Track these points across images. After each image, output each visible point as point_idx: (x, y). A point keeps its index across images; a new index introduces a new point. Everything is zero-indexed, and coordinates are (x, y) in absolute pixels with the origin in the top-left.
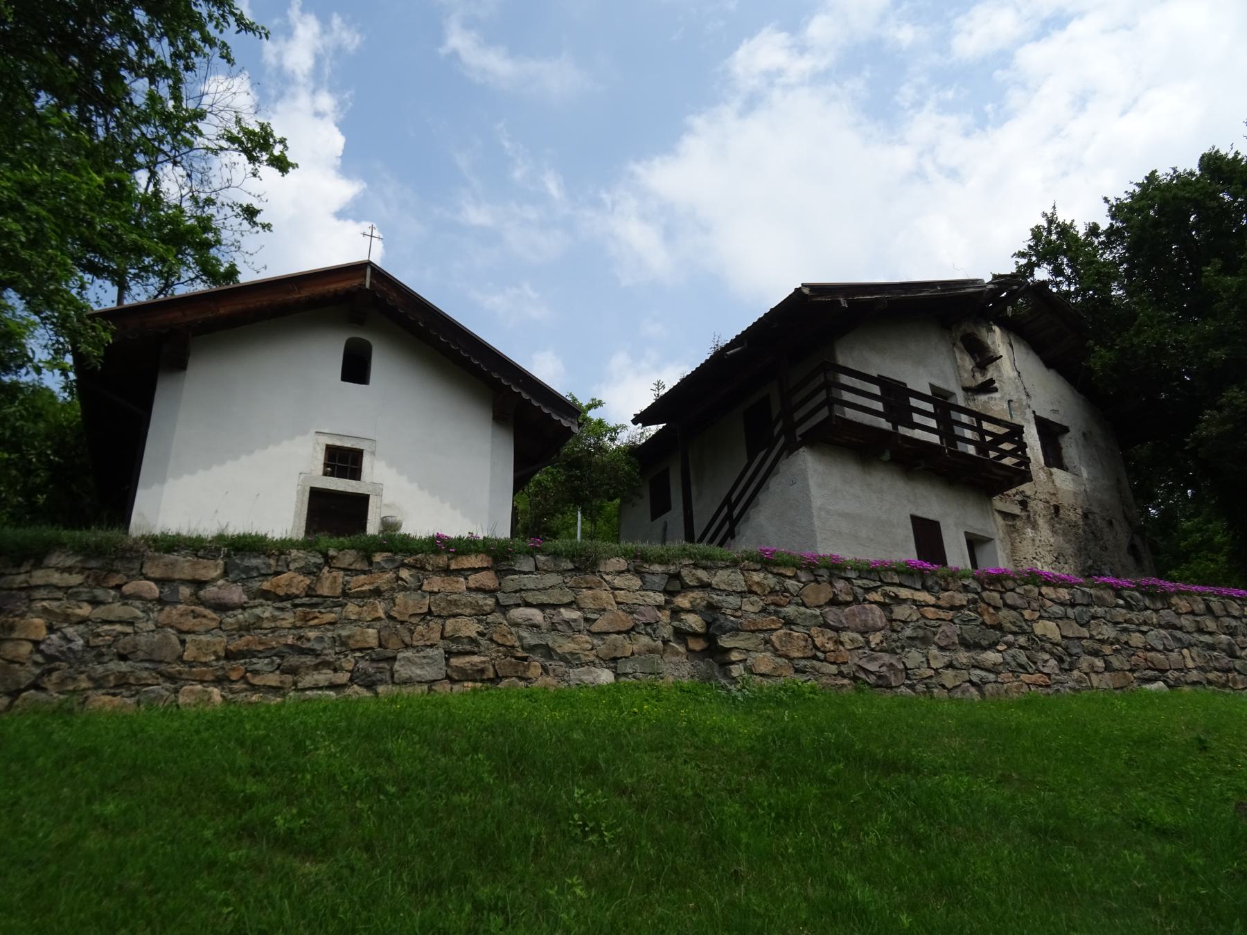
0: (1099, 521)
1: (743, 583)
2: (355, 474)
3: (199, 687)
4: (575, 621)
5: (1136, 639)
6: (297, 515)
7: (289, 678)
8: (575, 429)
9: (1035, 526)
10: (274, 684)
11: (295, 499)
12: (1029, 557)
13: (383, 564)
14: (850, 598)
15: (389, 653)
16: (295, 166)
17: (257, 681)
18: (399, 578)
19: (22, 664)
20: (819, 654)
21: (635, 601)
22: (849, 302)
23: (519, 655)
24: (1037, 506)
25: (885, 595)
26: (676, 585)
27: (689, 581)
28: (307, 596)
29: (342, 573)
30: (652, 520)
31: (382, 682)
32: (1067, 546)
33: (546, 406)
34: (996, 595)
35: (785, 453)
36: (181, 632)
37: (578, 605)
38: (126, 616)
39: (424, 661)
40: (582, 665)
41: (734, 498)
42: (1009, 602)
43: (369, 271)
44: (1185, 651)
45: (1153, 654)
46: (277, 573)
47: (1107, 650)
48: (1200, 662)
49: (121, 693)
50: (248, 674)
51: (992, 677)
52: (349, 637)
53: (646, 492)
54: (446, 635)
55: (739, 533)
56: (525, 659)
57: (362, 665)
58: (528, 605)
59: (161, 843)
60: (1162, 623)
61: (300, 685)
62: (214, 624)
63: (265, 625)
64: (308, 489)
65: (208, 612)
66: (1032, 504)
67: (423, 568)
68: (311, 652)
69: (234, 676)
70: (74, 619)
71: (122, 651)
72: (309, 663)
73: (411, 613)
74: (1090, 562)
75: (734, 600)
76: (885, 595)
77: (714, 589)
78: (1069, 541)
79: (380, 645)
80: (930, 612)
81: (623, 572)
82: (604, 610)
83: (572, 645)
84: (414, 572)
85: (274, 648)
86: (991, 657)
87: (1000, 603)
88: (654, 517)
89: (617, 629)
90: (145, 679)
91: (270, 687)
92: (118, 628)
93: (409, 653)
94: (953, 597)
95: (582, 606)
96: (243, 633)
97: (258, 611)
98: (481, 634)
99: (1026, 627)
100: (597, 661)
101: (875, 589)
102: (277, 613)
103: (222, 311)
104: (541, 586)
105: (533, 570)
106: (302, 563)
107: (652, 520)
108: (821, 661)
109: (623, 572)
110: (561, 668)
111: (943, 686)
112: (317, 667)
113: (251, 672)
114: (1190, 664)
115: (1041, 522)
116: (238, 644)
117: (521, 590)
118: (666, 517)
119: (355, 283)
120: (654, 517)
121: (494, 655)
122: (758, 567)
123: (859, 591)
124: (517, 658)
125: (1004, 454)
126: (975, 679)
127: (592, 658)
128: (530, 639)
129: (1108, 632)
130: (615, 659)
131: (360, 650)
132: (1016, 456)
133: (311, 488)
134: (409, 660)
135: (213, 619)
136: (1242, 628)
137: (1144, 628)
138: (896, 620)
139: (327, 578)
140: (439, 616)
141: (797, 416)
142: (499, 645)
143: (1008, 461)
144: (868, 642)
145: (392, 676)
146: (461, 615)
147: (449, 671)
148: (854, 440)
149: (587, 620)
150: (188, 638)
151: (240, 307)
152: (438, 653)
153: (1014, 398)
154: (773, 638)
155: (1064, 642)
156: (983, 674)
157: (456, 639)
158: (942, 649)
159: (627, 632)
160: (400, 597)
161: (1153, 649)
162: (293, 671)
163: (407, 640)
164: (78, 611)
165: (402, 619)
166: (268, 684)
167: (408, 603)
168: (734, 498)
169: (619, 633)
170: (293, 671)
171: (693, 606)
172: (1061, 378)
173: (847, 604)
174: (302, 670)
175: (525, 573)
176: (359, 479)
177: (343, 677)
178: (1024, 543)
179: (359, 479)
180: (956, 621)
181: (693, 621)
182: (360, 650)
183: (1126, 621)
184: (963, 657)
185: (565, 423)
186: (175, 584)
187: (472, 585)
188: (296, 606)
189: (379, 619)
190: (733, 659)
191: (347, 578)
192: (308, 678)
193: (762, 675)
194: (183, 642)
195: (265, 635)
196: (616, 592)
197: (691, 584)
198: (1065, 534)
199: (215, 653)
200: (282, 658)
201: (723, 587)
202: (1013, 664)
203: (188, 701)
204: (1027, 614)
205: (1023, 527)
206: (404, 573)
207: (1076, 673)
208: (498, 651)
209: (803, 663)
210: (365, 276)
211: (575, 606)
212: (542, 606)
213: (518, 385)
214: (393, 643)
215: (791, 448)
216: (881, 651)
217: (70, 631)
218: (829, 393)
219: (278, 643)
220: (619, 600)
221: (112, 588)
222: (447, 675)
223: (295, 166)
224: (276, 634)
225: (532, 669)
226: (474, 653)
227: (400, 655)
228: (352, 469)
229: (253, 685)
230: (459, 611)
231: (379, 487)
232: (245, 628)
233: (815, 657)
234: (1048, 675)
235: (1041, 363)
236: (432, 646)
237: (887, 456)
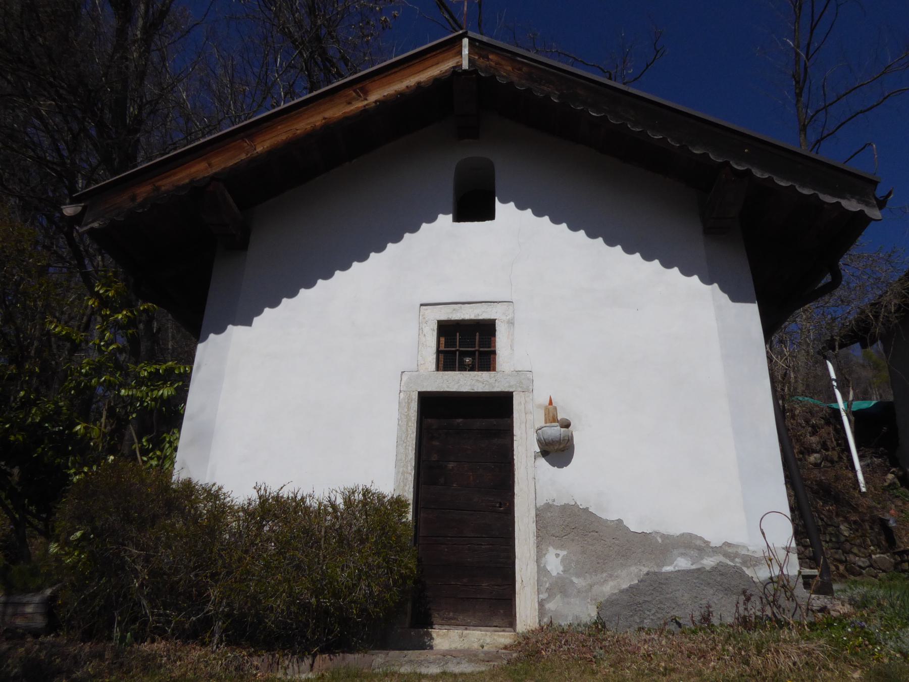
6: (400, 442)
8: (874, 213)
11: (396, 415)
16: (783, 548)
33: (804, 185)
53: (694, 567)
59: (674, 606)
64: (415, 397)
103: (259, 149)
122: (29, 615)
133: (420, 393)
151: (284, 137)
176: (494, 370)
179: (494, 370)
185: (851, 205)
210: (460, 53)
223: (783, 548)
228: (481, 353)
231: (526, 378)
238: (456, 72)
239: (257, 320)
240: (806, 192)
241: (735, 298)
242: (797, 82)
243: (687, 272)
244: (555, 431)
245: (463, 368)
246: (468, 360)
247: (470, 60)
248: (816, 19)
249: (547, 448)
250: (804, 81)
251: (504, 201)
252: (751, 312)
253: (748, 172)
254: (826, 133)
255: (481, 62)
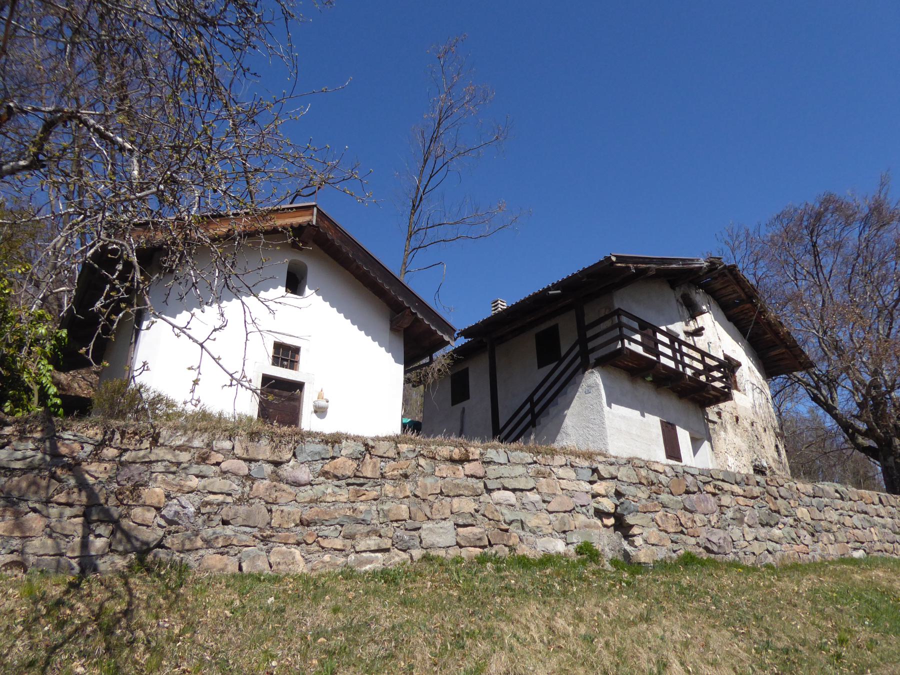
0: (759, 428)
1: (636, 477)
2: (293, 364)
3: (284, 548)
4: (537, 502)
5: (848, 521)
7: (349, 542)
9: (725, 430)
10: (339, 547)
12: (723, 451)
13: (407, 454)
14: (696, 489)
15: (417, 525)
17: (325, 543)
18: (418, 465)
19: (148, 526)
20: (684, 530)
21: (574, 489)
22: (636, 268)
23: (502, 527)
24: (726, 416)
25: (715, 487)
26: (595, 477)
27: (604, 473)
28: (355, 476)
29: (379, 459)
30: (453, 404)
31: (414, 547)
32: (743, 444)
33: (433, 325)
34: (774, 489)
35: (581, 370)
36: (267, 503)
37: (537, 490)
38: (225, 489)
39: (441, 531)
40: (544, 536)
41: (536, 398)
42: (782, 494)
43: (315, 209)
44: (872, 529)
45: (856, 531)
46: (333, 458)
47: (835, 528)
48: (881, 538)
49: (228, 552)
50: (319, 539)
51: (778, 546)
52: (389, 511)
54: (454, 511)
55: (540, 424)
56: (507, 531)
57: (399, 533)
58: (505, 489)
60: (859, 510)
61: (358, 549)
62: (291, 498)
63: (329, 499)
65: (286, 487)
66: (723, 414)
67: (434, 458)
68: (363, 522)
69: (310, 541)
70: (186, 489)
71: (225, 518)
72: (362, 531)
73: (429, 493)
74: (755, 456)
75: (632, 489)
76: (715, 487)
77: (619, 481)
78: (744, 442)
79: (410, 518)
80: (741, 500)
81: (563, 466)
82: (555, 494)
83: (537, 521)
84: (428, 461)
85: (336, 518)
86: (776, 532)
87: (777, 495)
88: (455, 402)
89: (564, 509)
90: (245, 541)
91: (335, 550)
92: (220, 498)
93: (430, 525)
94: (752, 490)
95: (540, 491)
96: (314, 505)
97: (322, 487)
98: (477, 511)
99: (792, 512)
100: (554, 533)
101: (708, 483)
102: (337, 489)
104: (513, 475)
105: (507, 462)
106: (351, 451)
107: (453, 404)
108: (685, 534)
109: (563, 466)
110: (532, 538)
111: (754, 554)
112: (368, 534)
113: (321, 537)
114: (876, 539)
115: (729, 427)
116: (308, 514)
117: (501, 477)
118: (465, 404)
119: (307, 218)
120: (455, 402)
121: (487, 527)
123: (699, 483)
124: (502, 530)
125: (715, 379)
126: (771, 549)
127: (550, 531)
128: (509, 517)
129: (834, 516)
130: (564, 532)
131: (397, 521)
132: (723, 382)
134: (431, 530)
135: (290, 493)
136: (897, 515)
137: (851, 513)
138: (723, 506)
139: (370, 464)
140: (448, 496)
141: (591, 345)
142: (490, 520)
143: (718, 385)
144: (710, 521)
145: (421, 542)
146: (462, 495)
147: (459, 539)
148: (630, 364)
149: (544, 501)
150: (274, 508)
152: (449, 524)
153: (712, 341)
154: (657, 518)
155: (813, 523)
156: (774, 544)
157: (459, 514)
158: (750, 526)
159: (570, 511)
160: (420, 480)
161: (857, 528)
162: (351, 537)
163: (429, 514)
164: (189, 483)
165: (424, 498)
166: (335, 547)
167: (430, 484)
168: (536, 398)
169: (565, 512)
170: (351, 537)
171: (606, 492)
172: (736, 328)
173: (694, 493)
174: (358, 536)
175: (501, 464)
177: (387, 543)
178: (720, 441)
180: (755, 507)
181: (608, 505)
182: (397, 521)
183: (841, 509)
184: (763, 532)
186: (260, 463)
187: (468, 473)
188: (348, 485)
189: (408, 497)
190: (636, 533)
191: (383, 464)
192: (363, 543)
193: (653, 545)
194: (270, 511)
195: (329, 507)
196: (561, 481)
197: (605, 476)
198: (742, 437)
199: (294, 520)
200: (342, 526)
201: (625, 479)
202: (789, 538)
203: (278, 560)
204: (792, 502)
205: (719, 431)
206: (422, 461)
207: (820, 543)
208: (489, 524)
209: (677, 536)
211: (535, 490)
212: (514, 490)
213: (415, 308)
214: (420, 516)
215: (585, 367)
216: (719, 528)
217: (184, 500)
218: (621, 330)
219: (339, 514)
220: (563, 487)
221: (214, 465)
222: (457, 542)
224: (336, 506)
225: (513, 538)
226: (472, 525)
227: (424, 526)
228: (291, 361)
229: (323, 548)
230: (461, 492)
232: (315, 501)
233: (682, 532)
234: (807, 545)
235: (725, 317)
236: (445, 519)
237: (649, 379)
238: (309, 224)
239: (178, 316)
240: (433, 328)
241: (396, 361)
242: (414, 206)
243: (381, 345)
244: (322, 403)
245: (283, 366)
246: (285, 363)
247: (316, 221)
248: (437, 168)
249: (318, 410)
250: (418, 206)
251: (310, 288)
252: (401, 368)
253: (416, 313)
254: (422, 245)
255: (321, 224)
